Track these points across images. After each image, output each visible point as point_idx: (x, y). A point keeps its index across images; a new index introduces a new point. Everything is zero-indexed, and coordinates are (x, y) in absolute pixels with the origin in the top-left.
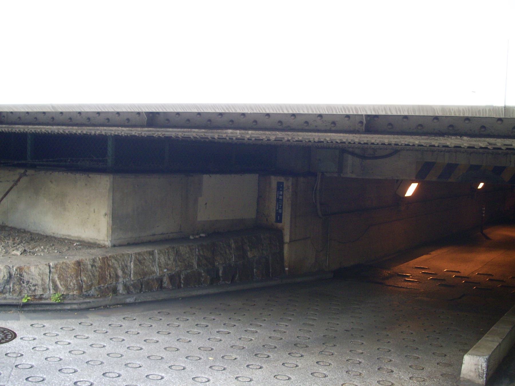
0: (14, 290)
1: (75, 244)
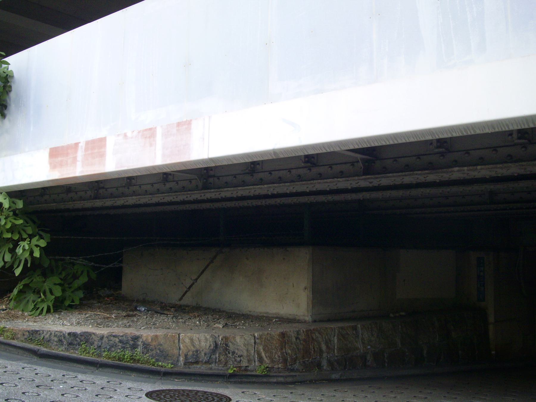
0: (219, 361)
1: (274, 320)
